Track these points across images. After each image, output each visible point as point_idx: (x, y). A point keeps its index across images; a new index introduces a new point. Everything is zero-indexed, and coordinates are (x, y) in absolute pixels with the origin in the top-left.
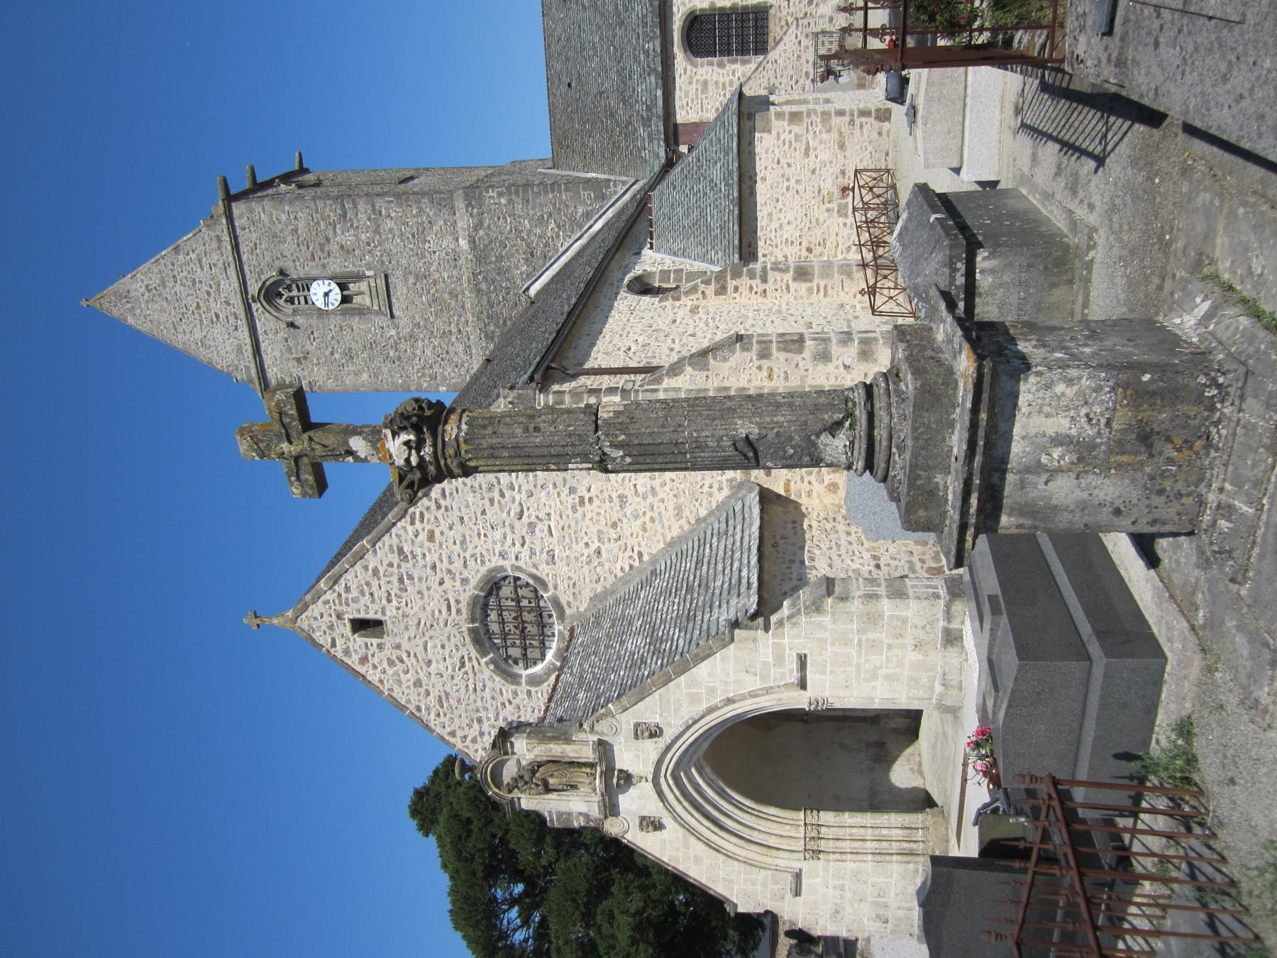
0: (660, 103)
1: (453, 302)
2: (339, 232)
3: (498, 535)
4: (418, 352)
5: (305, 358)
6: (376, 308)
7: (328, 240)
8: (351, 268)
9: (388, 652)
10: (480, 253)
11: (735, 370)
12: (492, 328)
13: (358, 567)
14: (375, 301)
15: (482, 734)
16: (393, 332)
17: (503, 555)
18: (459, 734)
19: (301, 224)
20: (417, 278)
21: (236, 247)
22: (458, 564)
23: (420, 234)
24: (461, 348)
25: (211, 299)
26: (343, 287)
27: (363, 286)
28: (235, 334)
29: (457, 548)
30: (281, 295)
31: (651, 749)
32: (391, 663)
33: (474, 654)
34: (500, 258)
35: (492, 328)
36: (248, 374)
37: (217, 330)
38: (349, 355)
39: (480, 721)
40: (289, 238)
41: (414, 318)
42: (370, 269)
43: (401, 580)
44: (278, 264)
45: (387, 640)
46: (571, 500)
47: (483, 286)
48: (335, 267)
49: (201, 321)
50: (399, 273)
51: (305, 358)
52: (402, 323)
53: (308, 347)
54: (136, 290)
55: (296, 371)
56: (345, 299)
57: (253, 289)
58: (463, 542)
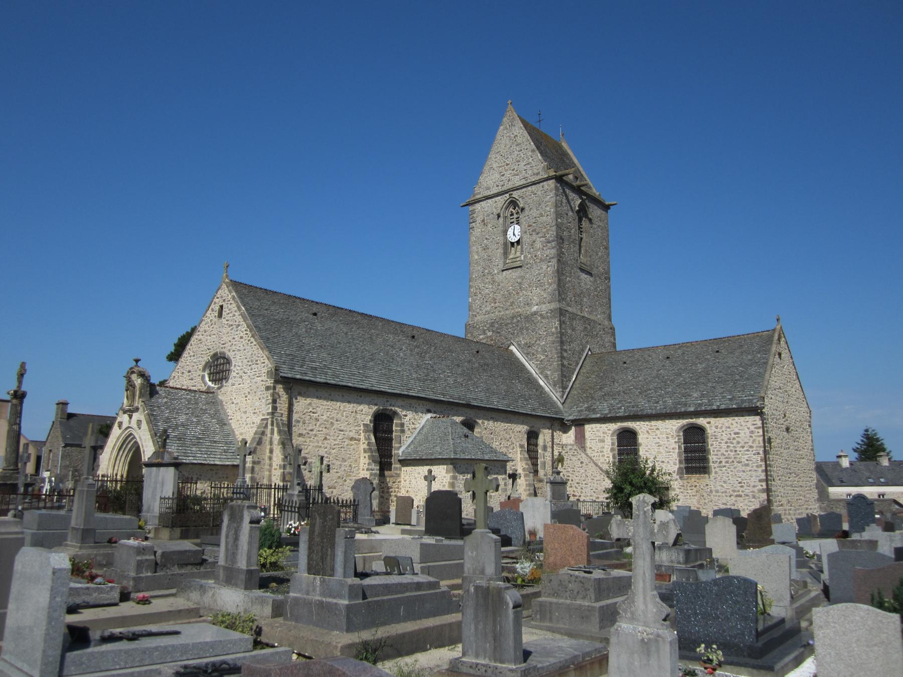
0: (594, 416)
7: (538, 234)
10: (530, 318)
20: (520, 283)
21: (534, 183)
23: (540, 285)
24: (488, 309)
26: (518, 242)
27: (518, 254)
34: (527, 329)
36: (479, 193)
37: (497, 176)
38: (485, 248)
44: (527, 207)
47: (515, 320)
50: (523, 274)
53: (489, 225)
56: (512, 244)
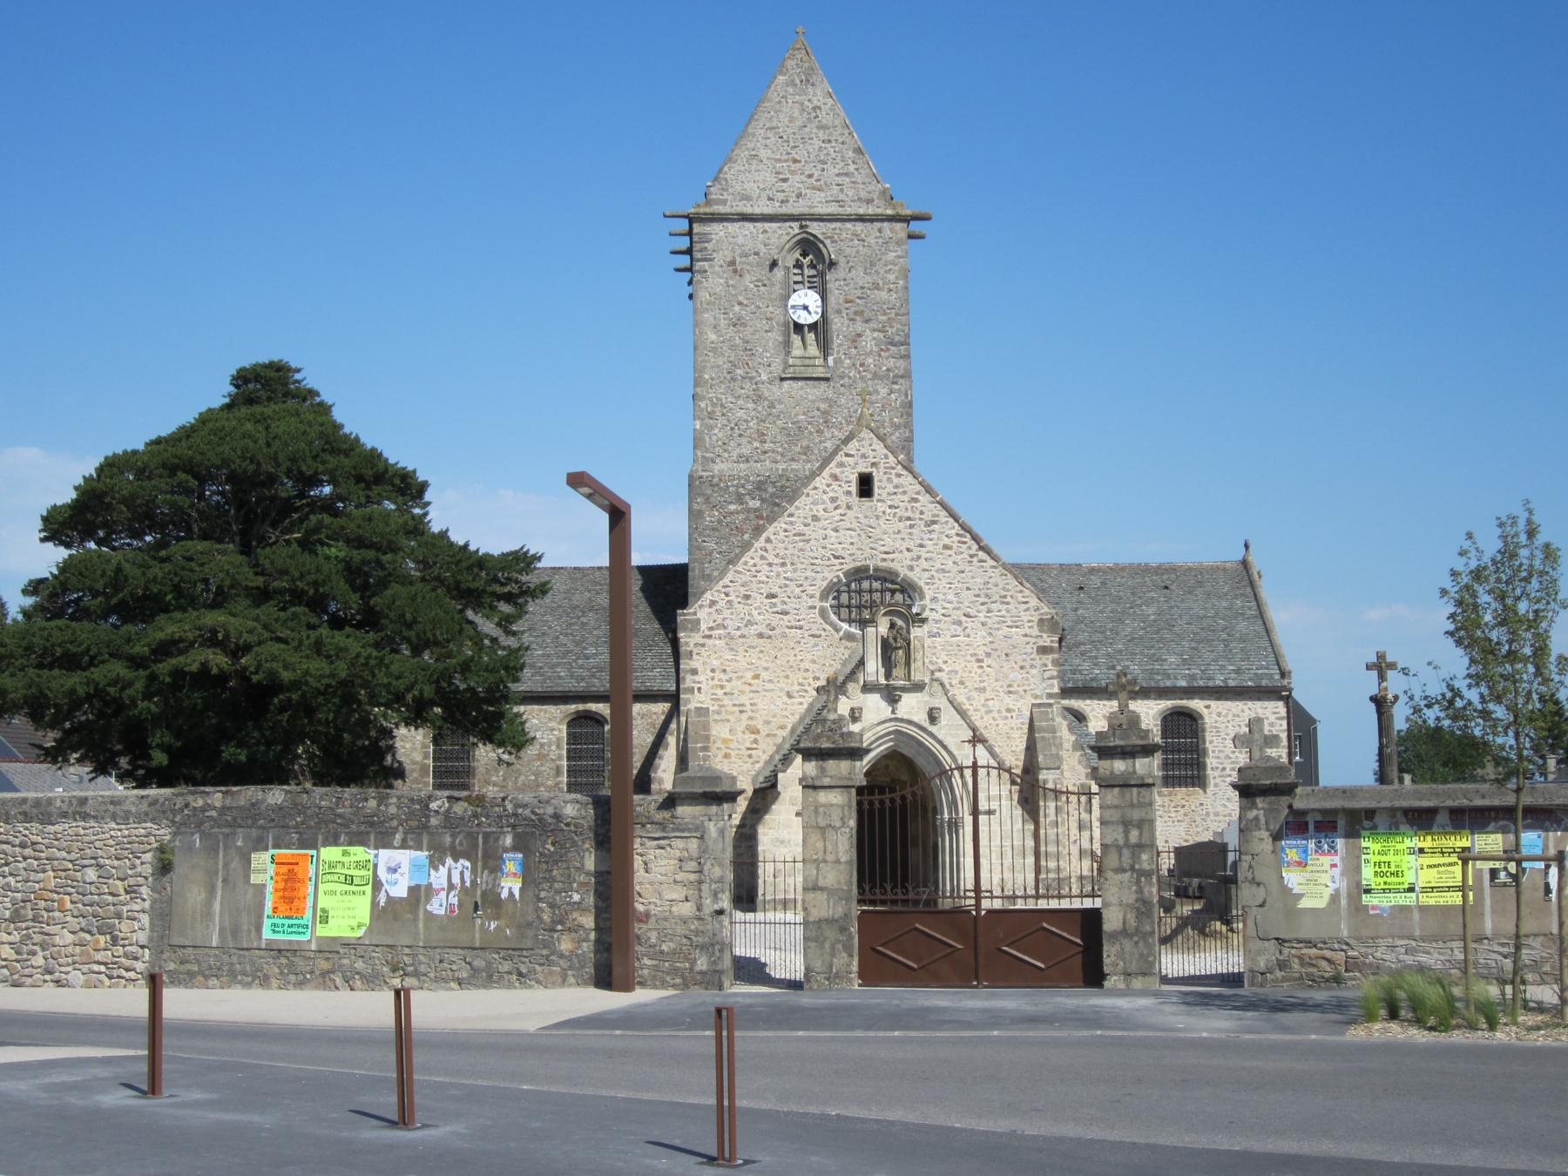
1: (798, 449)
2: (876, 334)
3: (951, 597)
4: (740, 402)
5: (735, 271)
6: (791, 361)
7: (867, 321)
8: (836, 342)
9: (843, 500)
11: (1073, 769)
12: (771, 490)
13: (919, 487)
14: (798, 362)
15: (770, 565)
16: (764, 377)
17: (934, 599)
18: (768, 546)
19: (884, 295)
20: (825, 413)
21: (861, 219)
22: (925, 565)
24: (746, 451)
25: (803, 178)
26: (813, 327)
27: (813, 350)
28: (764, 195)
29: (938, 566)
30: (804, 255)
31: (921, 718)
32: (833, 500)
33: (846, 567)
35: (771, 490)
36: (718, 202)
37: (771, 179)
39: (783, 564)
40: (869, 279)
41: (780, 402)
42: (835, 362)
43: (909, 519)
44: (842, 261)
45: (855, 499)
46: (981, 653)
48: (838, 324)
49: (779, 160)
51: (735, 271)
52: (775, 389)
53: (748, 278)
54: (815, 94)
55: (720, 258)
56: (798, 328)
57: (815, 228)
58: (944, 571)
